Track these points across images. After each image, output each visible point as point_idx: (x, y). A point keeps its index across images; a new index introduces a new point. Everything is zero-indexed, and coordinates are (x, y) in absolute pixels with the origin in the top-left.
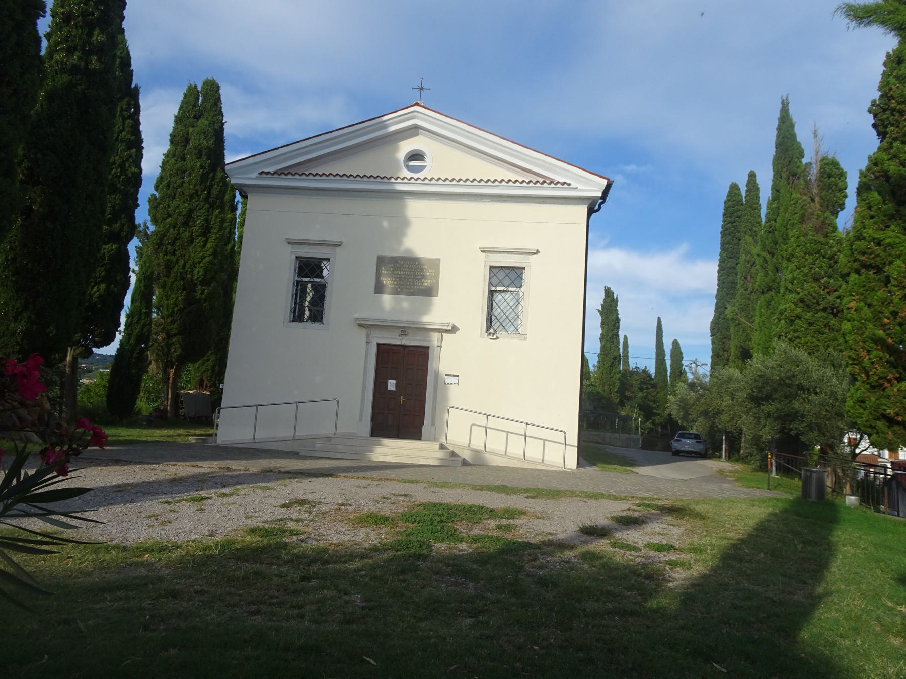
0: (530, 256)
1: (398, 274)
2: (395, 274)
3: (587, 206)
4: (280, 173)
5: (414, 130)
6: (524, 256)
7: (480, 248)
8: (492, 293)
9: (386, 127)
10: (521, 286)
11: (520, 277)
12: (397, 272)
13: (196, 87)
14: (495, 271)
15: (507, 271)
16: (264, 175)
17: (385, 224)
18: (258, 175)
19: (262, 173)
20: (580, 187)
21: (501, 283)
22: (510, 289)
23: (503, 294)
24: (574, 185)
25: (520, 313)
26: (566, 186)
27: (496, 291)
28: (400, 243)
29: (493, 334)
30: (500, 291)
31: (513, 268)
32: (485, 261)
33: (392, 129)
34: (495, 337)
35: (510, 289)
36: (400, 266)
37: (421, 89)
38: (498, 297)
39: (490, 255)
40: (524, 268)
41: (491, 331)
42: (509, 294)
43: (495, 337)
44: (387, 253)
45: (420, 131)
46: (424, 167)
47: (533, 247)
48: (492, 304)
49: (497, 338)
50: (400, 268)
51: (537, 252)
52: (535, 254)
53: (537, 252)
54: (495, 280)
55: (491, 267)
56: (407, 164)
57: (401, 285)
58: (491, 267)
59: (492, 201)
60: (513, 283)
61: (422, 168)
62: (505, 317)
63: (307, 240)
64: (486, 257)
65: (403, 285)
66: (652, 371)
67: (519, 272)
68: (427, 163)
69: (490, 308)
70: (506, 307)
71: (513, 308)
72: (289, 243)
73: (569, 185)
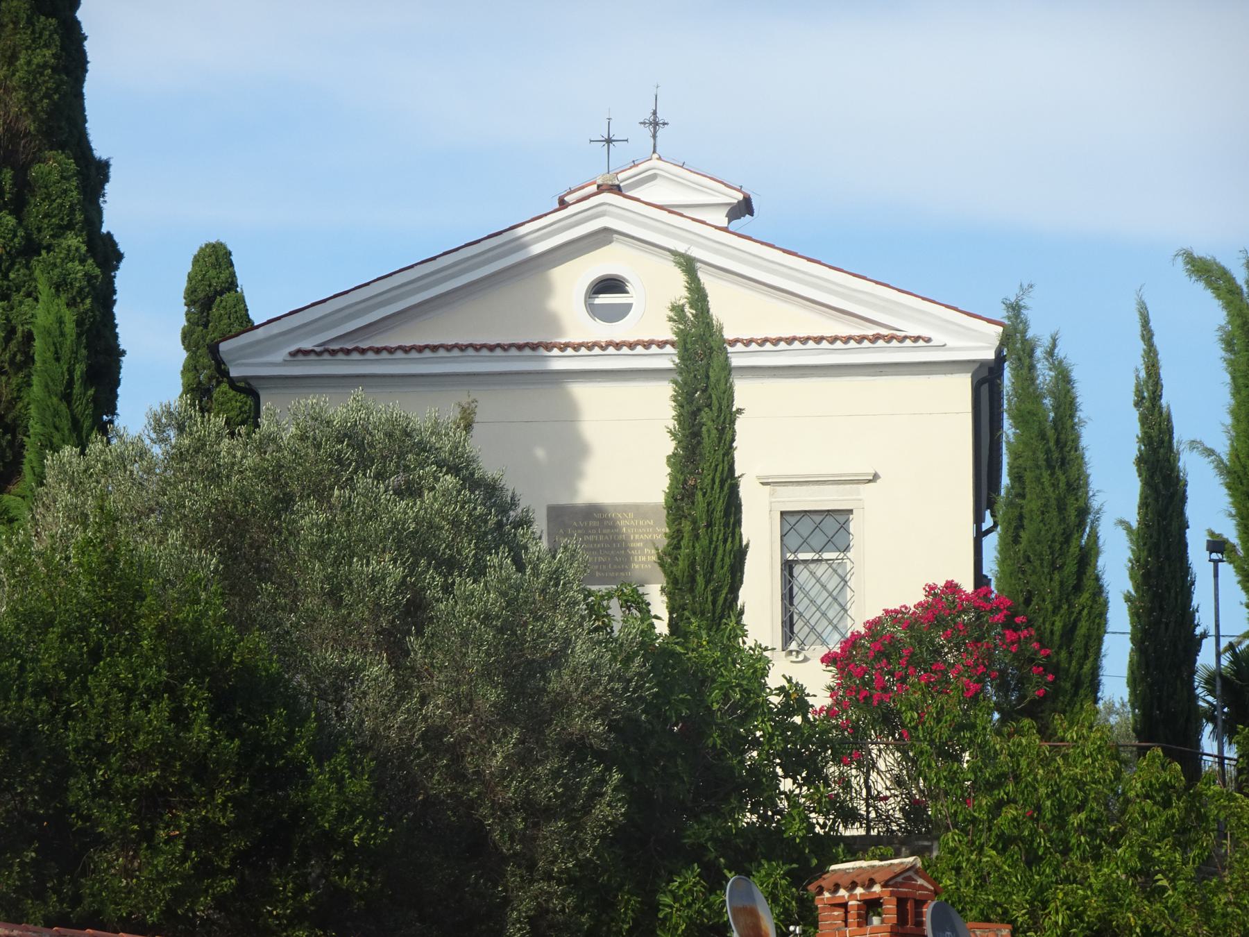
0: (861, 486)
1: (594, 542)
2: (588, 542)
3: (970, 375)
4: (326, 351)
5: (604, 237)
6: (848, 486)
7: (758, 477)
8: (788, 567)
9: (524, 246)
10: (847, 549)
11: (844, 527)
12: (591, 538)
13: (1128, 592)
14: (792, 520)
15: (818, 519)
16: (300, 357)
17: (540, 453)
18: (289, 358)
19: (299, 352)
20: (950, 344)
21: (805, 544)
22: (826, 556)
23: (812, 566)
24: (938, 339)
25: (849, 576)
26: (921, 343)
27: (797, 562)
28: (574, 491)
29: (798, 652)
30: (805, 561)
31: (829, 512)
32: (771, 503)
33: (537, 249)
34: (801, 657)
35: (826, 556)
36: (595, 523)
37: (609, 141)
38: (801, 574)
39: (779, 489)
40: (851, 511)
41: (793, 646)
42: (824, 566)
43: (801, 657)
44: (563, 500)
45: (615, 236)
46: (627, 308)
47: (867, 470)
48: (791, 589)
49: (806, 660)
50: (596, 528)
51: (876, 477)
52: (870, 481)
53: (876, 477)
54: (793, 541)
55: (782, 513)
56: (591, 301)
57: (602, 563)
58: (782, 513)
59: (774, 376)
60: (830, 544)
61: (622, 311)
62: (818, 615)
63: (841, 475)
64: (772, 495)
65: (606, 563)
66: (968, 586)
67: (842, 519)
68: (633, 296)
69: (788, 597)
70: (819, 593)
71: (824, 608)
72: (762, 483)
73: (928, 340)
